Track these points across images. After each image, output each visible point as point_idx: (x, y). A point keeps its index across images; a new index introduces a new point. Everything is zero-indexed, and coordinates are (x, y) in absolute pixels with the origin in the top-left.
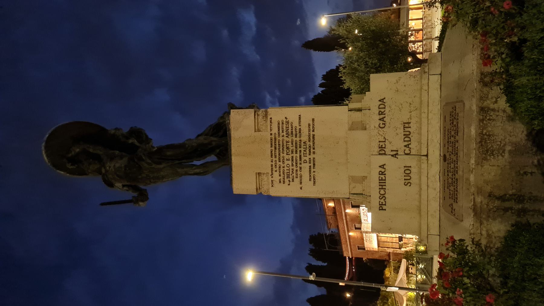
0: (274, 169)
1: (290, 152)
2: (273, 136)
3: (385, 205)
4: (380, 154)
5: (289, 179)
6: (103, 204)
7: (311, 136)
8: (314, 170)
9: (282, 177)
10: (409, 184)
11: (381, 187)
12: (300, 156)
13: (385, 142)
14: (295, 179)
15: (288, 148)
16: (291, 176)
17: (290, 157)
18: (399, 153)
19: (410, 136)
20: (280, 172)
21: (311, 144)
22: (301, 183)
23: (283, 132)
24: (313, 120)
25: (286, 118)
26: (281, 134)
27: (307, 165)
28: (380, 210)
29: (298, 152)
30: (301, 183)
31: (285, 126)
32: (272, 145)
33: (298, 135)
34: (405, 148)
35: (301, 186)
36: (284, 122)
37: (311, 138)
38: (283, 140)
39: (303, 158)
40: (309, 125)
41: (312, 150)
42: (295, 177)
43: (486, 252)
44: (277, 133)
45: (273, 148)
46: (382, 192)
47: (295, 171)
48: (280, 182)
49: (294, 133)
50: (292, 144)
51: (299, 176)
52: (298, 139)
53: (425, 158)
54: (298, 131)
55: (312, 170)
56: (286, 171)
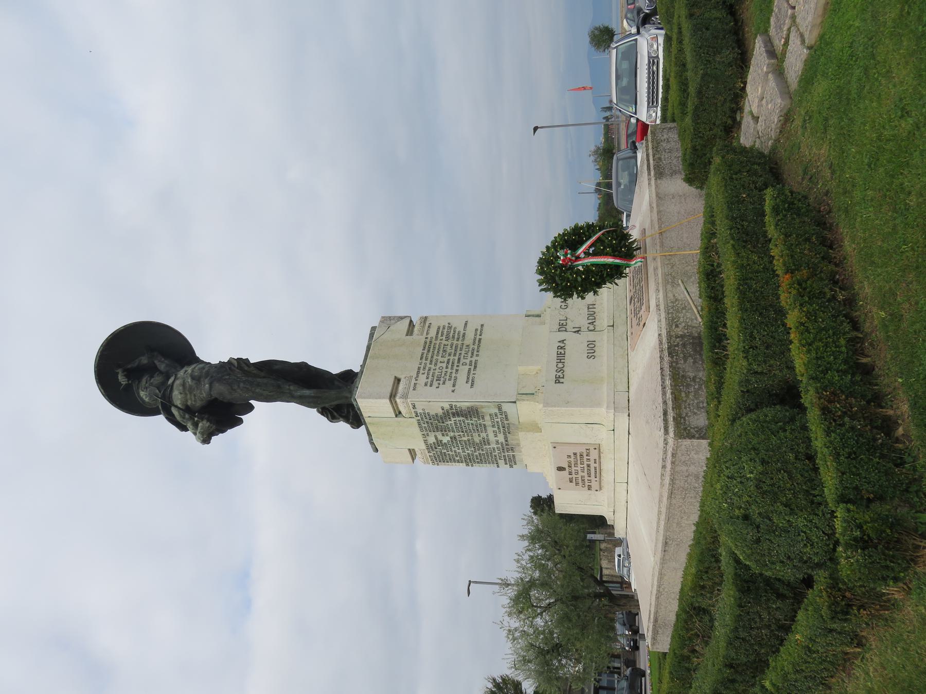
0: (421, 371)
1: (447, 355)
2: (428, 340)
3: (563, 378)
4: (559, 331)
5: (438, 382)
6: (376, 450)
7: (477, 340)
8: (474, 372)
9: (429, 380)
10: (593, 357)
11: (559, 361)
12: (459, 359)
13: (566, 320)
14: (447, 382)
15: (444, 351)
16: (442, 379)
17: (446, 360)
18: (582, 329)
19: (594, 315)
20: (428, 374)
21: (476, 347)
22: (454, 386)
23: (442, 336)
24: (482, 326)
25: (449, 324)
26: (440, 337)
27: (467, 367)
28: (556, 383)
29: (458, 355)
30: (454, 386)
31: (446, 330)
32: (424, 348)
33: (461, 339)
34: (589, 325)
35: (453, 389)
36: (446, 328)
37: (477, 342)
38: (440, 344)
39: (462, 361)
40: (476, 330)
41: (475, 353)
42: (447, 379)
43: (703, 407)
44: (434, 337)
45: (426, 351)
46: (560, 365)
47: (448, 374)
48: (426, 385)
49: (456, 337)
50: (451, 347)
51: (453, 378)
52: (460, 342)
53: (612, 328)
54: (461, 335)
55: (472, 372)
56: (437, 374)
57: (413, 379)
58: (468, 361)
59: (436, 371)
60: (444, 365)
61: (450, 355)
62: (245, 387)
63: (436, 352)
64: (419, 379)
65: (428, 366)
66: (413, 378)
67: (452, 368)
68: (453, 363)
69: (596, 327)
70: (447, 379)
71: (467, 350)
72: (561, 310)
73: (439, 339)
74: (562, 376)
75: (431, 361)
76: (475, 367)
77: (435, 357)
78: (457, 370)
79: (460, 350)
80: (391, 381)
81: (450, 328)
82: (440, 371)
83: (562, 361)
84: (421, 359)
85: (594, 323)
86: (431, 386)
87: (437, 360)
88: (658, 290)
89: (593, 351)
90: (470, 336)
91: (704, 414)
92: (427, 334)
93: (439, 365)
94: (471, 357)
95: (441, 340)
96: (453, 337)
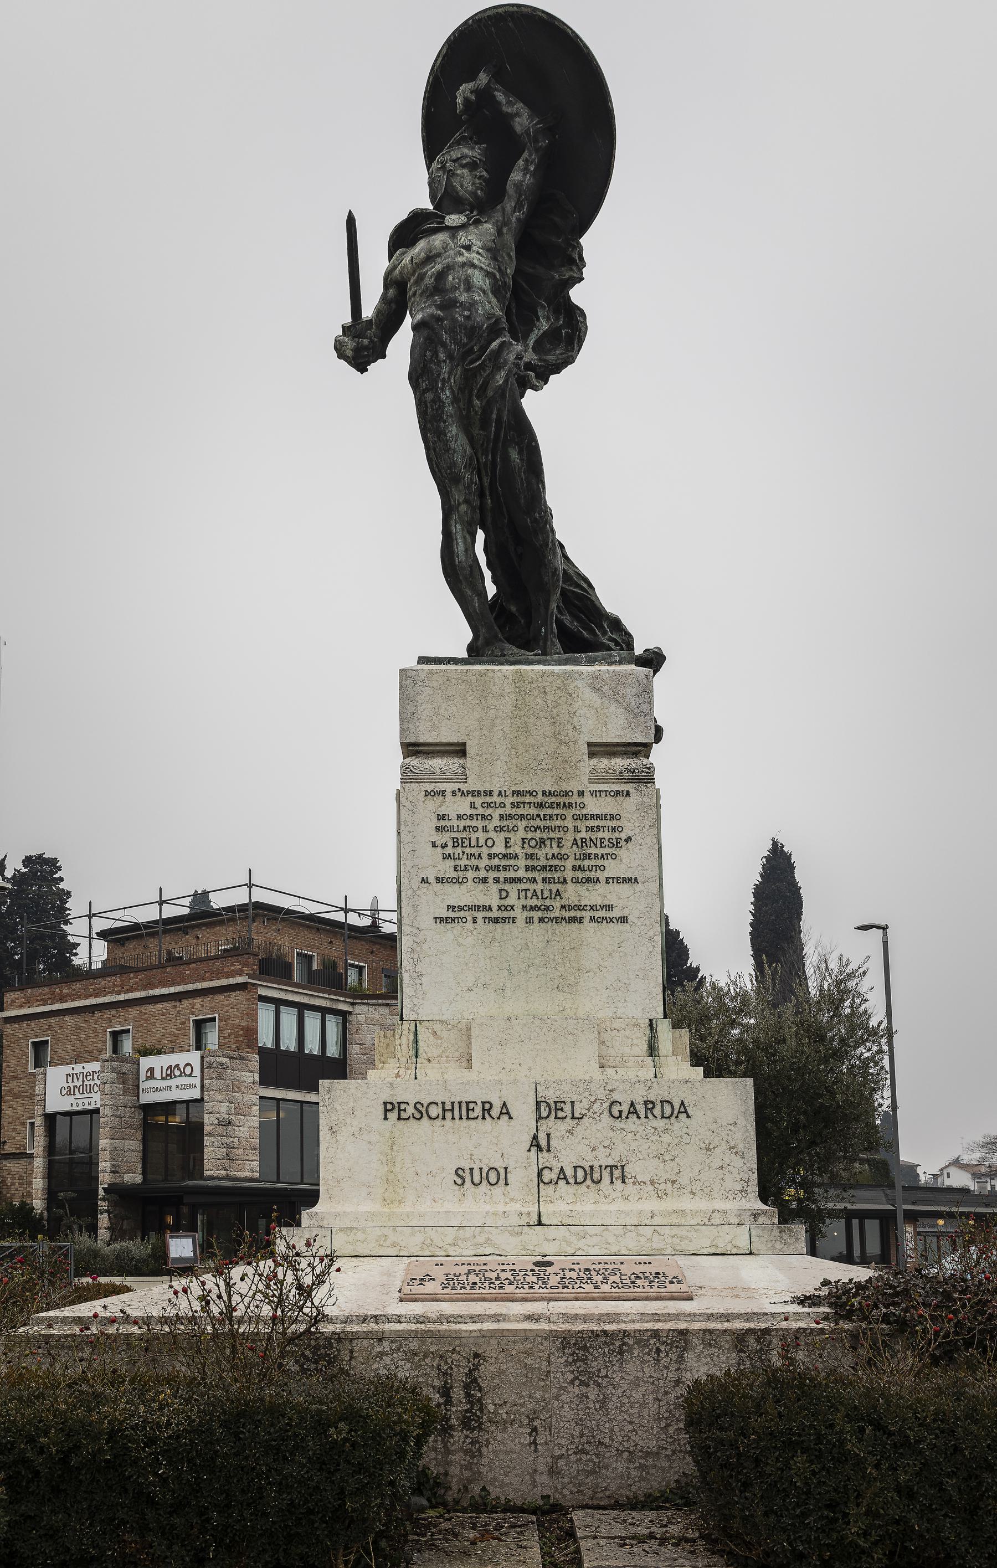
0: (478, 801)
2: (575, 799)
3: (399, 1119)
4: (538, 1104)
5: (450, 844)
7: (578, 914)
8: (480, 921)
9: (455, 823)
10: (459, 1181)
11: (448, 1107)
12: (518, 880)
14: (450, 863)
19: (589, 1182)
20: (471, 817)
21: (556, 913)
22: (440, 880)
24: (624, 920)
25: (628, 839)
26: (582, 825)
27: (495, 902)
28: (385, 1103)
29: (530, 875)
30: (440, 880)
31: (607, 835)
33: (579, 875)
34: (557, 1171)
38: (565, 828)
39: (513, 889)
40: (610, 908)
41: (536, 915)
42: (457, 862)
44: (584, 811)
45: (540, 798)
47: (474, 862)
48: (441, 817)
49: (586, 863)
52: (569, 874)
53: (534, 1220)
54: (593, 874)
56: (473, 836)
57: (455, 786)
58: (512, 900)
59: (480, 834)
60: (499, 848)
61: (530, 856)
62: (427, 407)
63: (538, 823)
64: (458, 798)
65: (496, 813)
66: (461, 786)
67: (489, 868)
68: (505, 868)
69: (551, 1187)
70: (457, 862)
71: (546, 894)
72: (606, 1105)
73: (578, 823)
74: (403, 1115)
75: (510, 817)
76: (496, 920)
77: (522, 824)
78: (484, 880)
79: (544, 880)
80: (448, 735)
81: (616, 844)
82: (481, 842)
83: (448, 1115)
84: (517, 793)
85: (562, 1183)
86: (438, 829)
87: (515, 829)
88: (530, 1317)
89: (477, 1180)
90: (592, 896)
91: (652, 1445)
92: (594, 793)
93: (499, 838)
94: (524, 907)
95: (576, 830)
96: (587, 856)
